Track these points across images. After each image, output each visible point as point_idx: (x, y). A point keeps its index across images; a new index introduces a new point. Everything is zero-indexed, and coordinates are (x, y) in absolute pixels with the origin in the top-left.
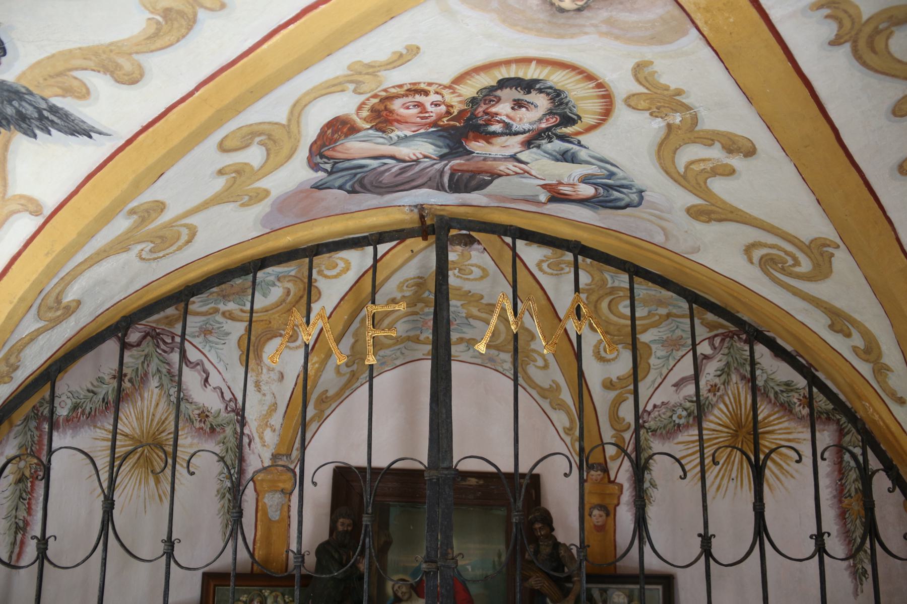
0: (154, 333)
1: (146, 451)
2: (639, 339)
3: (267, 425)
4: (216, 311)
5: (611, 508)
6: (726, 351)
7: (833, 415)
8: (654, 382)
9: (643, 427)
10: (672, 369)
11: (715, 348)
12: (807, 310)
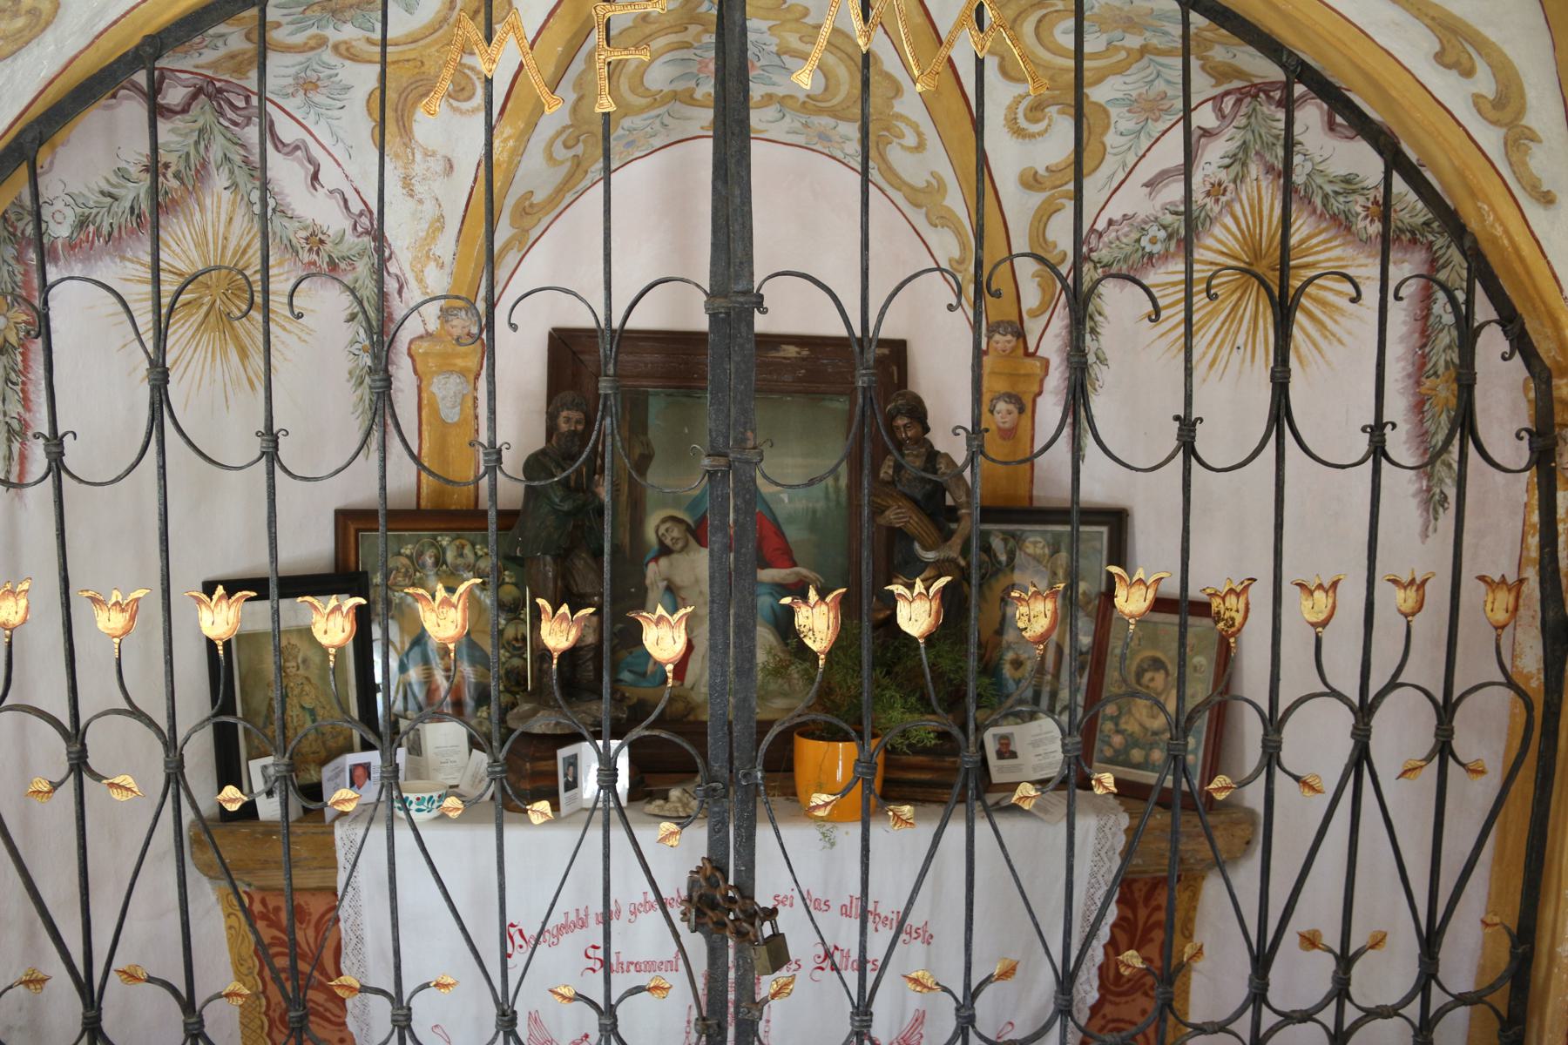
0: (211, 89)
1: (218, 302)
2: (1088, 97)
3: (428, 257)
4: (322, 42)
5: (1027, 400)
6: (1244, 121)
7: (1423, 236)
8: (1111, 177)
9: (1089, 259)
10: (1144, 156)
11: (1224, 117)
12: (1397, 24)
